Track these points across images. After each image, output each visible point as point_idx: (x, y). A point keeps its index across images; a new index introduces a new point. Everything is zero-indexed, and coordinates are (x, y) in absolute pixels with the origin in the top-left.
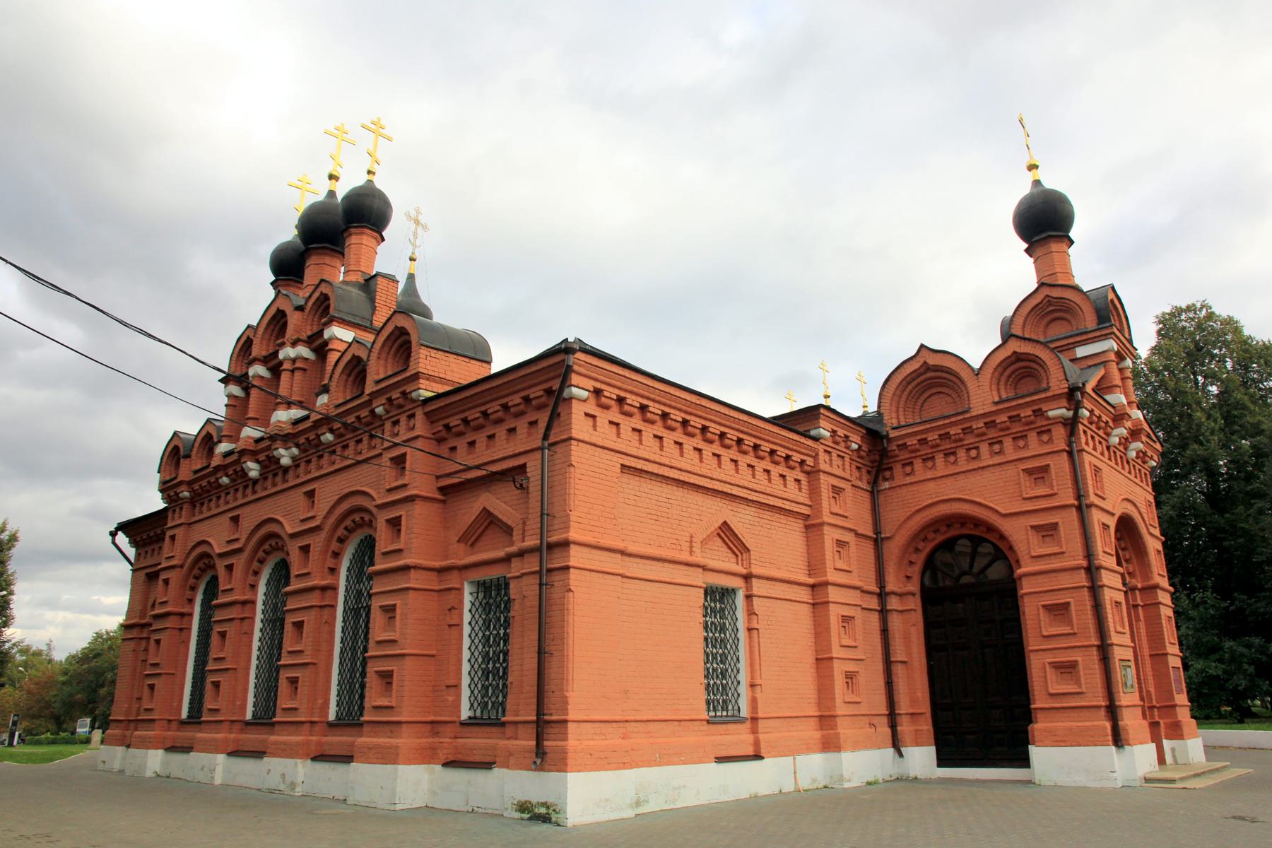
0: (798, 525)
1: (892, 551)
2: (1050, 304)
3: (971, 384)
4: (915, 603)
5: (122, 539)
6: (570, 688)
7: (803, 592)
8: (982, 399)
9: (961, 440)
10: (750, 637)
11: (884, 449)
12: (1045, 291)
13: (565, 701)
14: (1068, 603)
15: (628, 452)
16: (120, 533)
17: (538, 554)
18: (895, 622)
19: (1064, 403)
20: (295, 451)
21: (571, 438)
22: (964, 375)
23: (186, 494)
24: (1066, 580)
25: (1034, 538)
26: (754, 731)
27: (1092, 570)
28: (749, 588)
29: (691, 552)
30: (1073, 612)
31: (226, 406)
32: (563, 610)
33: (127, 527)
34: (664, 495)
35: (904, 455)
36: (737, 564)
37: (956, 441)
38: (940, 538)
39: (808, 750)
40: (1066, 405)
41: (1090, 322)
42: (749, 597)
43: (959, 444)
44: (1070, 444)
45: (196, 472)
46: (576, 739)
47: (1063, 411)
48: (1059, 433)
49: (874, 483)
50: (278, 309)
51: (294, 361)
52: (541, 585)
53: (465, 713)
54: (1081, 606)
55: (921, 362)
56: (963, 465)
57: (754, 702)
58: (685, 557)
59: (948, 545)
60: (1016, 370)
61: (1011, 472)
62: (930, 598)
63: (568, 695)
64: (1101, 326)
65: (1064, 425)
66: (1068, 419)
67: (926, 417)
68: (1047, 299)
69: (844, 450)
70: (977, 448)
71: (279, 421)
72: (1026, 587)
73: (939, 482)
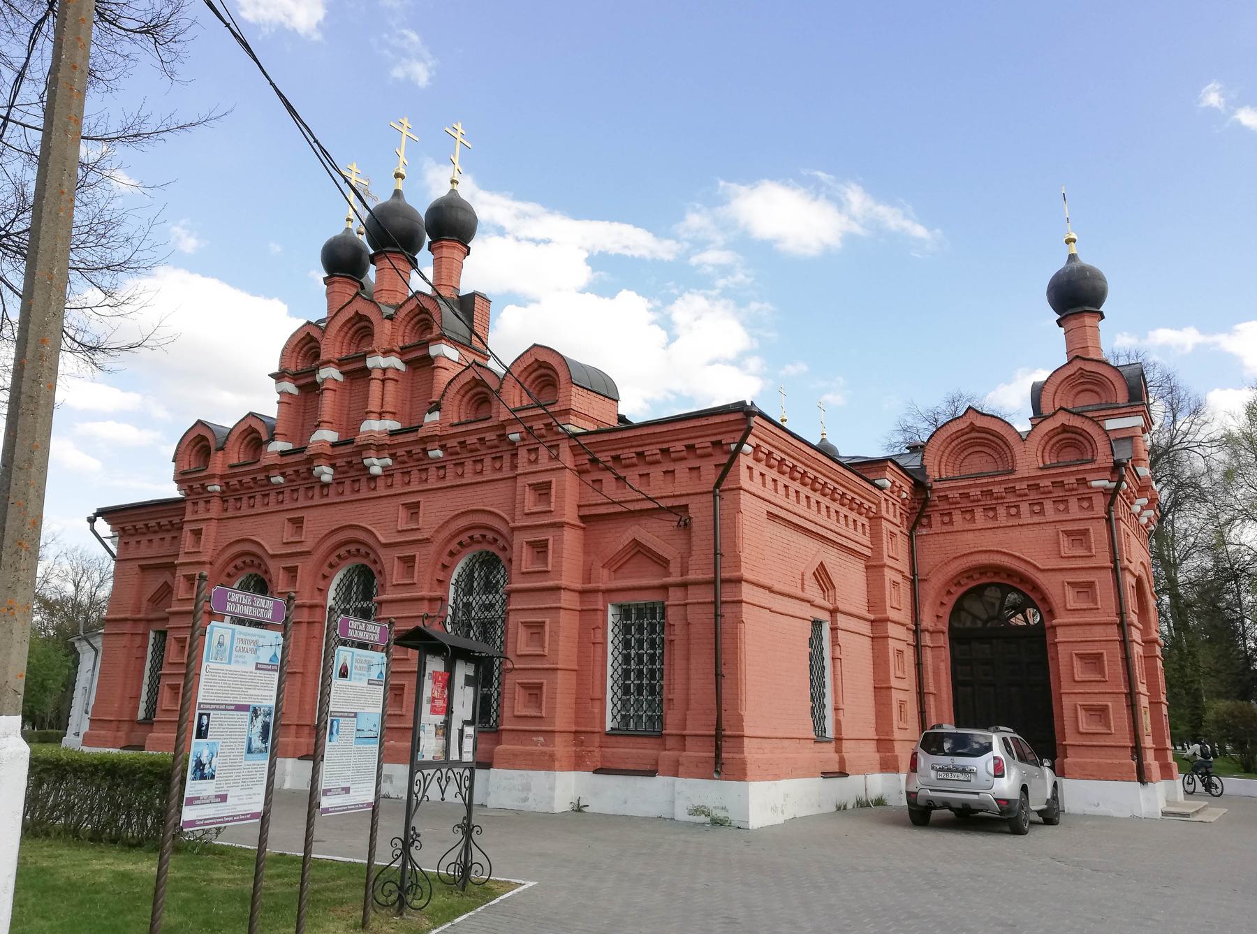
0: (860, 565)
1: (930, 591)
2: (1082, 376)
3: (1018, 449)
4: (944, 640)
5: (103, 527)
6: (743, 708)
7: (866, 626)
8: (1028, 462)
9: (1002, 498)
10: (834, 667)
11: (927, 499)
12: (1078, 364)
13: (740, 719)
14: (1101, 654)
15: (772, 501)
16: (99, 519)
17: (713, 586)
18: (928, 656)
19: (1108, 475)
20: (389, 461)
21: (740, 488)
22: (1011, 439)
23: (217, 488)
24: (1098, 633)
25: (1070, 593)
26: (838, 750)
27: (1123, 626)
28: (834, 621)
29: (803, 589)
30: (1106, 662)
31: (278, 403)
32: (735, 638)
33: (106, 513)
34: (787, 538)
35: (943, 506)
36: (824, 599)
37: (997, 498)
38: (972, 584)
39: (872, 771)
40: (1110, 477)
41: (1122, 398)
42: (834, 629)
43: (1000, 501)
44: (1108, 512)
45: (232, 467)
46: (752, 751)
47: (1106, 483)
48: (1099, 503)
49: (912, 529)
50: (357, 313)
51: (384, 370)
52: (716, 615)
53: (609, 725)
54: (1111, 655)
55: (968, 424)
56: (1003, 519)
57: (838, 724)
58: (798, 593)
59: (978, 591)
60: (1061, 440)
61: (1050, 531)
62: (958, 638)
63: (742, 713)
64: (1133, 404)
65: (1104, 494)
66: (1109, 489)
67: (965, 471)
68: (1080, 372)
69: (896, 498)
70: (1017, 507)
71: (372, 431)
72: (1061, 635)
73: (977, 533)
